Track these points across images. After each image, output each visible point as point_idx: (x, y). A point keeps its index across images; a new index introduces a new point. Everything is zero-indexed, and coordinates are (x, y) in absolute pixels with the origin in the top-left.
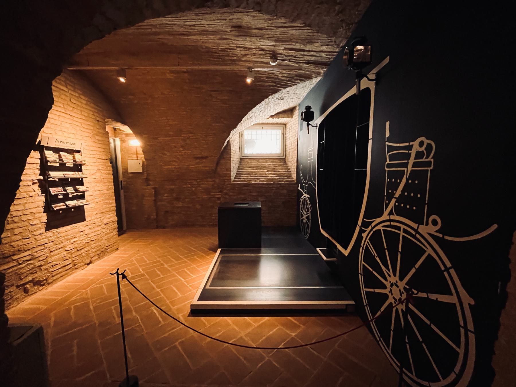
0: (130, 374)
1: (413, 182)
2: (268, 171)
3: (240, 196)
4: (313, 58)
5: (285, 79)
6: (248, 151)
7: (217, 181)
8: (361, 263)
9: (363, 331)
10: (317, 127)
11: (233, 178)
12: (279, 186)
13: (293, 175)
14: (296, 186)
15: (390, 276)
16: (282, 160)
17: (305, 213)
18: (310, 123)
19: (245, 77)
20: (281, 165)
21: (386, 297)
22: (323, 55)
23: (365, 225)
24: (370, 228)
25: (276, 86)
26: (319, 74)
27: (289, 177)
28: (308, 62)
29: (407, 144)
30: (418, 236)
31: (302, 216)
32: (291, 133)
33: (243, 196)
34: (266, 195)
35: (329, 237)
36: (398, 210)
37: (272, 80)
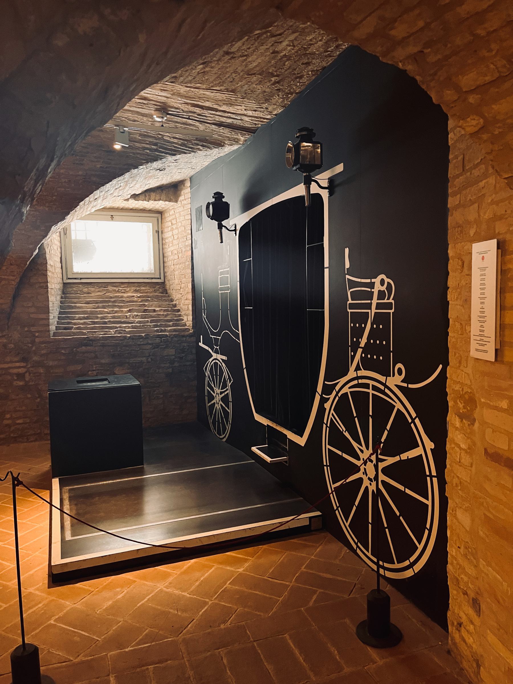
0: (26, 642)
1: (378, 326)
2: (130, 311)
3: (71, 368)
4: (229, 121)
5: (176, 141)
6: (80, 266)
7: (16, 336)
8: (326, 447)
9: (336, 546)
10: (235, 230)
11: (53, 328)
12: (158, 340)
13: (185, 318)
14: (193, 339)
15: (362, 451)
16: (157, 287)
17: (219, 391)
18: (224, 223)
19: (113, 140)
20: (157, 297)
21: (357, 469)
22: (246, 119)
23: (328, 390)
24: (334, 393)
25: (156, 150)
26: (237, 141)
27: (178, 321)
28: (220, 125)
29: (368, 281)
30: (387, 391)
31: (212, 398)
32: (175, 232)
33: (79, 367)
34: (132, 360)
35: (270, 424)
36: (366, 364)
37: (151, 140)
